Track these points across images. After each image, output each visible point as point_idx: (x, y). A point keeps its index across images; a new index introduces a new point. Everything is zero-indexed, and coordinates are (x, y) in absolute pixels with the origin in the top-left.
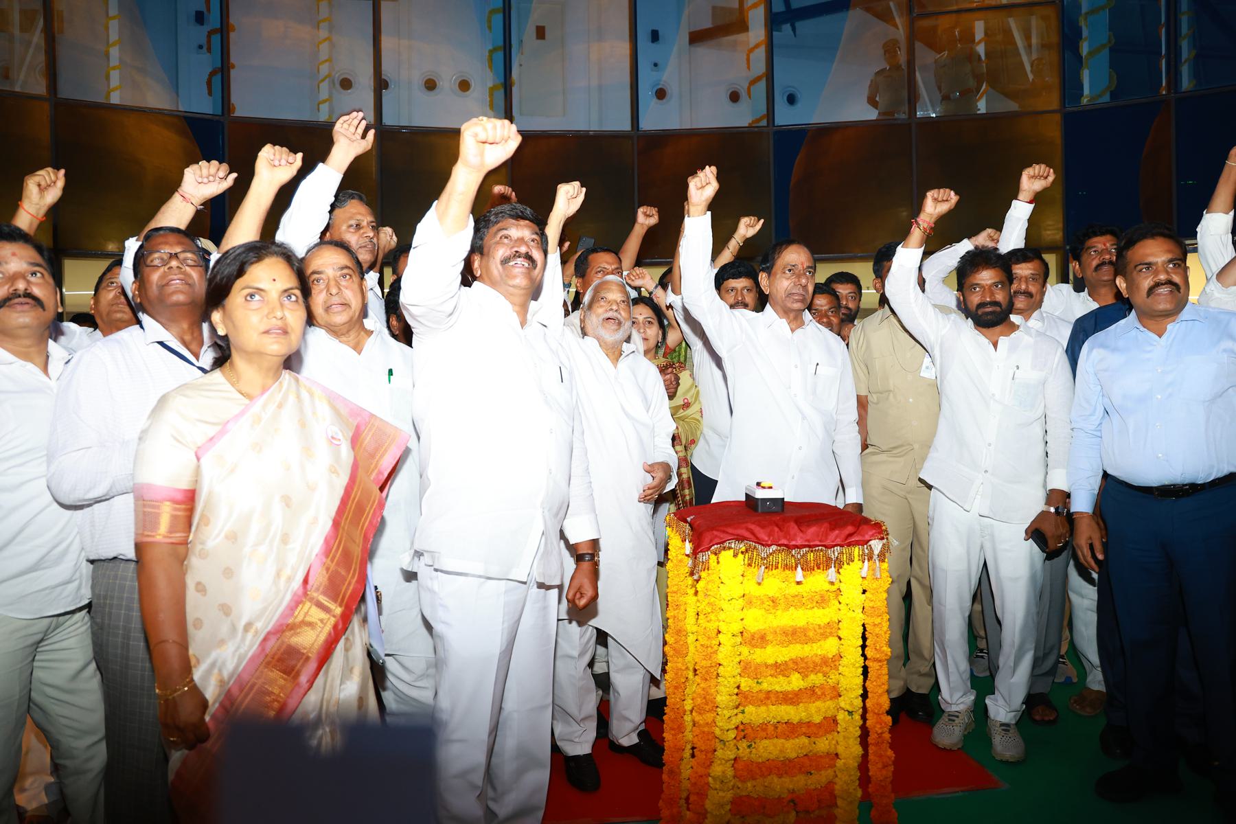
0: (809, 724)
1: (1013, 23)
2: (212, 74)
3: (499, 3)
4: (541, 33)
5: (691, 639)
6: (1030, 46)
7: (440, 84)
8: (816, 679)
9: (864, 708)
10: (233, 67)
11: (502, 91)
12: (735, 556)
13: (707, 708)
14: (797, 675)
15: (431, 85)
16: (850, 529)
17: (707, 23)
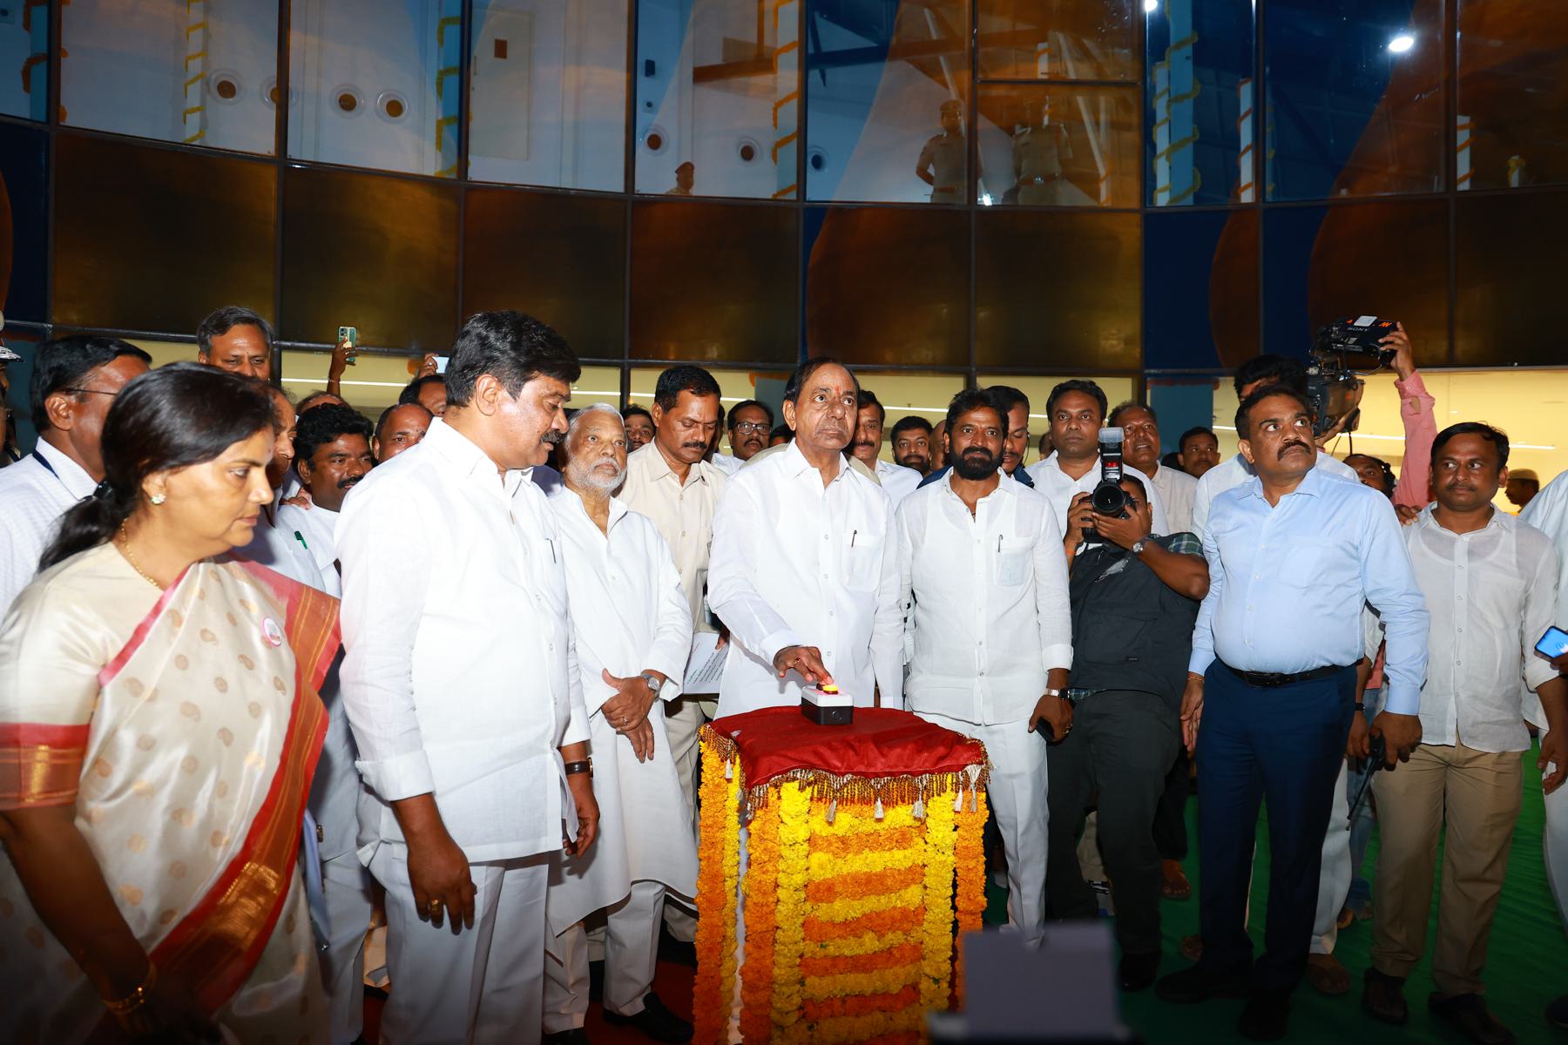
0: (886, 995)
1: (1081, 101)
2: (32, 61)
3: (455, 10)
4: (501, 49)
5: (730, 884)
6: (1097, 123)
7: (360, 101)
8: (894, 938)
9: (954, 974)
10: (66, 54)
11: (455, 127)
12: (802, 789)
13: (762, 984)
14: (871, 935)
15: (347, 103)
16: (941, 750)
17: (715, 58)
